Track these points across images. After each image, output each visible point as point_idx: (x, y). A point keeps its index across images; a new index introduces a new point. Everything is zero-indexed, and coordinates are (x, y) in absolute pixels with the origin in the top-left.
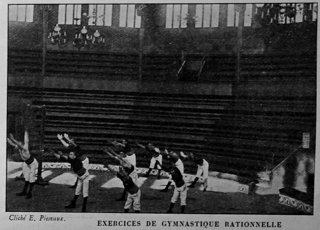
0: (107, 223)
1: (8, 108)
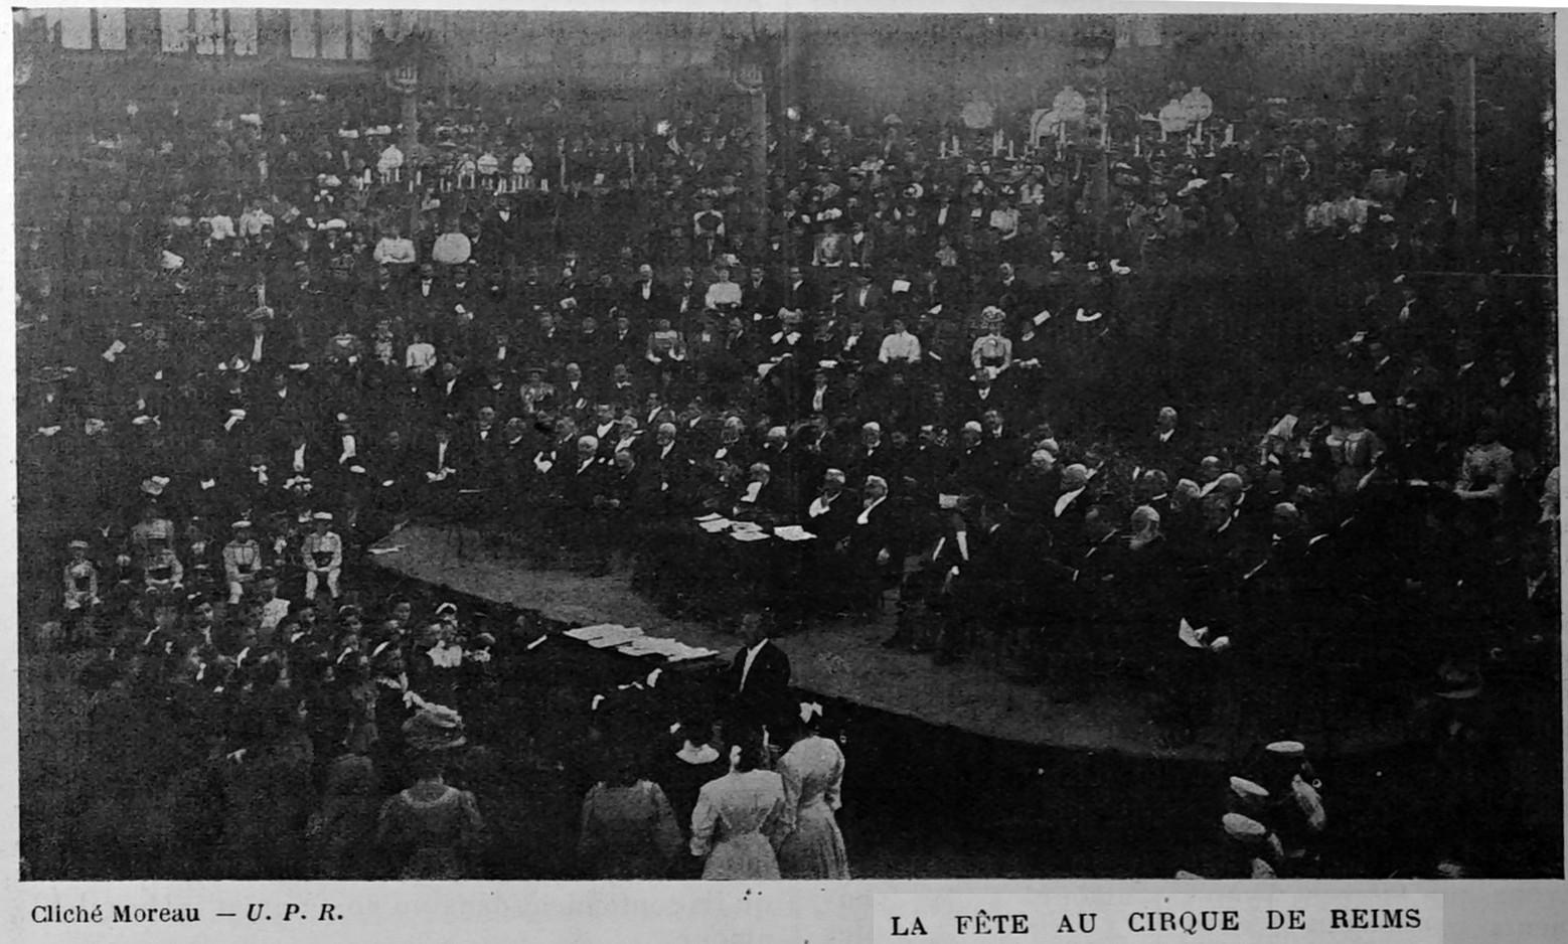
1: (22, 490)
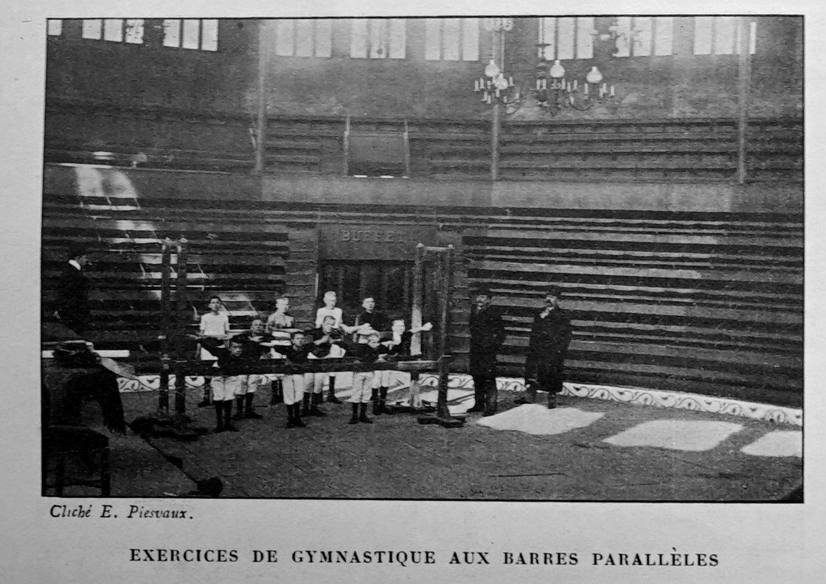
0: (155, 555)
